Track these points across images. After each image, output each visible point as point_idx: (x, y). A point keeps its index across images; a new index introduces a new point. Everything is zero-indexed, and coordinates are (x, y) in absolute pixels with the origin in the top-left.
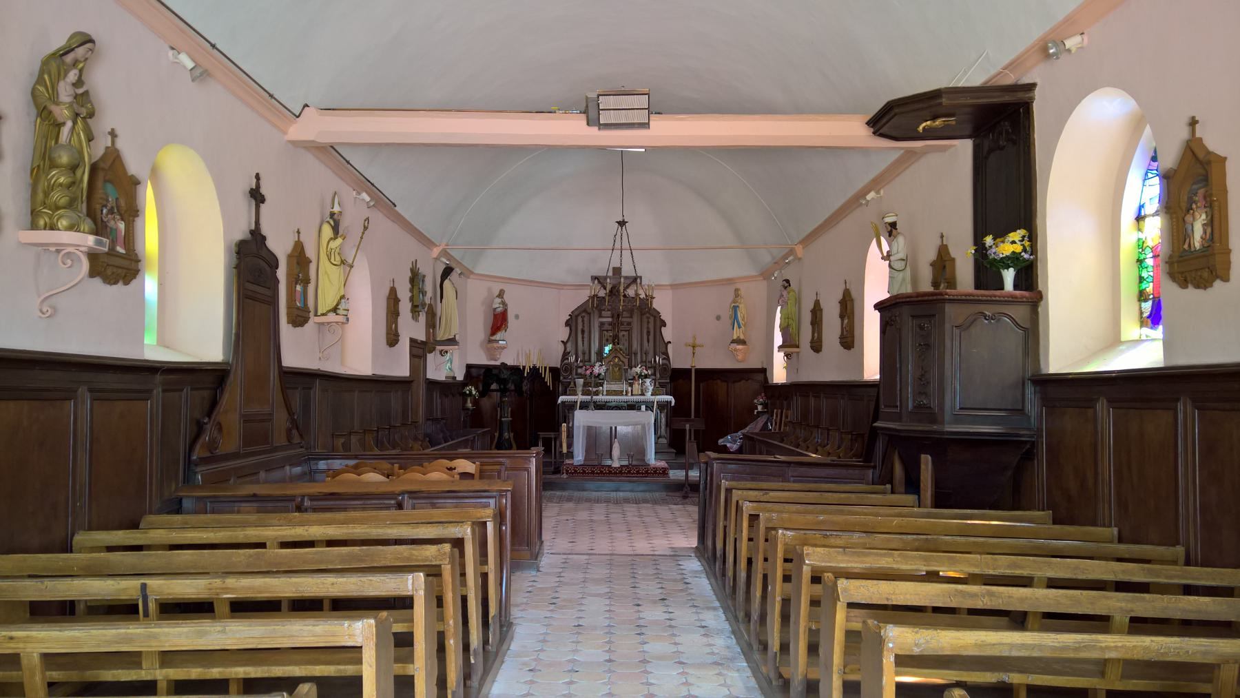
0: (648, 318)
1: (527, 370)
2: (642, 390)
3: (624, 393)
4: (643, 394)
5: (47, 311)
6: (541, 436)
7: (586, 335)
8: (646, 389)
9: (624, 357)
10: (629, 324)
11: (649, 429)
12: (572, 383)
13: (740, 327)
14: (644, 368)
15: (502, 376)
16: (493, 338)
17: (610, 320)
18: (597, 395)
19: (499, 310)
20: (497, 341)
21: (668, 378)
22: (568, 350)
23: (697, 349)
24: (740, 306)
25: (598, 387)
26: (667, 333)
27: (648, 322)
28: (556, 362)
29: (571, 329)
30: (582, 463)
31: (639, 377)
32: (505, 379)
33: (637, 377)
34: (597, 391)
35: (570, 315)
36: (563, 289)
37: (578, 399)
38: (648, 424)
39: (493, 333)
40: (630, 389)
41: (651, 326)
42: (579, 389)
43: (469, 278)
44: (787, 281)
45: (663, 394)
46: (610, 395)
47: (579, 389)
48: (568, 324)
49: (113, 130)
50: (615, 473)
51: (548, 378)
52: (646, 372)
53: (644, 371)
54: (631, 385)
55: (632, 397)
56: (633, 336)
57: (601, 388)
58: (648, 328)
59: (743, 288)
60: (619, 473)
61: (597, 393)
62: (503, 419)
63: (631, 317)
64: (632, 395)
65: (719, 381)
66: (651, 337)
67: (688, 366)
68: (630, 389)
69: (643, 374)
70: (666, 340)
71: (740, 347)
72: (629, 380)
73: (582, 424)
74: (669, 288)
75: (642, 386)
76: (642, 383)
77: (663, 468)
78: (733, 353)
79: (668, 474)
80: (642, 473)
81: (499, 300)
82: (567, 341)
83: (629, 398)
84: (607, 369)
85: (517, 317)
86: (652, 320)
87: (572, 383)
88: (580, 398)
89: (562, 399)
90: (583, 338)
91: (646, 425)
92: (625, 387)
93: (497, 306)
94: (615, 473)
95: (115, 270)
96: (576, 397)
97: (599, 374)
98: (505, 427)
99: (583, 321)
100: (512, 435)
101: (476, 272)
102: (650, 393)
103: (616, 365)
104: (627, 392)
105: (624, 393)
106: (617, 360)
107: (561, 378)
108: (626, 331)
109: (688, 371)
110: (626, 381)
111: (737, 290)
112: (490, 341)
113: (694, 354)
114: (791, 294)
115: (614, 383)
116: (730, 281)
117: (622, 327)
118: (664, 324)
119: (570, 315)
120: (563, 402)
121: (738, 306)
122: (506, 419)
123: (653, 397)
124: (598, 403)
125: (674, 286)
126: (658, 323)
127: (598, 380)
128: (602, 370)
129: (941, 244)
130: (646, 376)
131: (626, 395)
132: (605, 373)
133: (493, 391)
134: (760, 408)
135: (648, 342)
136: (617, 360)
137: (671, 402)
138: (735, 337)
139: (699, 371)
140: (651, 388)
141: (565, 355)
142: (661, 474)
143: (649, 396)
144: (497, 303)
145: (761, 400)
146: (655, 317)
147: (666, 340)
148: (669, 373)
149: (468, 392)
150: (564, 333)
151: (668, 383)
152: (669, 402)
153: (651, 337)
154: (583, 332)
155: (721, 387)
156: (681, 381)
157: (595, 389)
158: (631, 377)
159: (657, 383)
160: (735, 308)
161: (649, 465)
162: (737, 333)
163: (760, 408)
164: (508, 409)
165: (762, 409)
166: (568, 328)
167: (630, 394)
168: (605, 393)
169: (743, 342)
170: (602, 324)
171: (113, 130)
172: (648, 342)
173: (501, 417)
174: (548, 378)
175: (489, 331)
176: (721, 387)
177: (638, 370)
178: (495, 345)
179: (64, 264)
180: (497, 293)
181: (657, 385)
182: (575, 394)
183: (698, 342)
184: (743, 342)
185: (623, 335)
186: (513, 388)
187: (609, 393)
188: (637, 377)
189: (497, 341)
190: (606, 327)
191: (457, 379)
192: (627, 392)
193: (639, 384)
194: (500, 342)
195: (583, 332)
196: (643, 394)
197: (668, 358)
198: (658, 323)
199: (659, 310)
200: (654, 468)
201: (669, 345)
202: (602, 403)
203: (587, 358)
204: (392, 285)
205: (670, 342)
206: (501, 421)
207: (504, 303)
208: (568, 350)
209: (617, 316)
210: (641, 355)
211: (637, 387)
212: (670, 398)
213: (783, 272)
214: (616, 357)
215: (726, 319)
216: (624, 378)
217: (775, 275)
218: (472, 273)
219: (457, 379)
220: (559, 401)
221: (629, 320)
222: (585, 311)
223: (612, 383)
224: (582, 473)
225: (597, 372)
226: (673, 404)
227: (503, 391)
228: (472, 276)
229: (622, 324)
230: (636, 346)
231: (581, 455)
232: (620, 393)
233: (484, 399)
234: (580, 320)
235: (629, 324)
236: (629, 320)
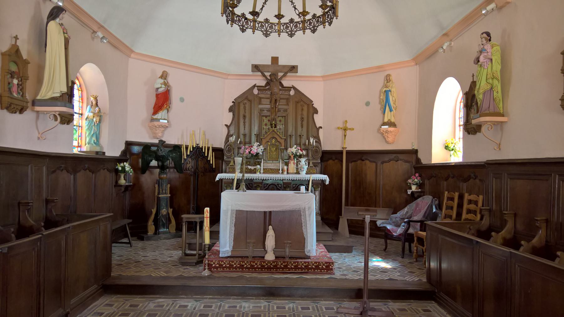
0: (302, 106)
1: (190, 148)
2: (297, 169)
3: (281, 172)
4: (298, 173)
5: (44, 137)
6: (184, 220)
7: (247, 120)
8: (302, 168)
9: (281, 138)
10: (286, 110)
11: (310, 215)
12: (232, 162)
13: (391, 110)
14: (299, 148)
15: (160, 153)
16: (155, 117)
17: (269, 106)
18: (255, 173)
19: (161, 90)
20: (158, 120)
21: (319, 159)
22: (231, 133)
23: (348, 132)
24: (392, 90)
25: (256, 165)
26: (319, 120)
27: (302, 110)
28: (220, 144)
29: (234, 115)
30: (229, 254)
31: (294, 157)
32: (163, 157)
33: (292, 157)
34: (255, 169)
35: (233, 102)
36: (227, 79)
37: (235, 177)
38: (309, 208)
39: (155, 112)
40: (285, 168)
41: (305, 113)
42: (238, 167)
43: (130, 57)
44: (488, 34)
45: (317, 173)
46: (267, 173)
47: (238, 167)
48: (231, 109)
49: (17, 36)
50: (269, 268)
51: (211, 157)
52: (301, 153)
53: (300, 151)
54: (287, 164)
55: (288, 176)
56: (289, 121)
57: (259, 166)
58: (302, 114)
59: (394, 75)
60: (273, 268)
61: (254, 172)
62: (160, 196)
63: (288, 104)
64: (288, 173)
65: (367, 162)
66: (305, 123)
67: (338, 148)
68: (285, 168)
69: (298, 154)
70: (318, 126)
71: (392, 129)
72: (285, 160)
73: (230, 207)
74: (321, 79)
75: (297, 166)
76: (297, 162)
77: (326, 263)
78: (383, 135)
79: (332, 269)
80: (302, 268)
81: (162, 81)
82: (230, 125)
83: (285, 176)
84: (265, 149)
85: (182, 100)
86: (305, 108)
87: (232, 162)
88: (237, 175)
89: (219, 176)
90: (244, 123)
91: (306, 210)
92: (281, 165)
93: (159, 86)
94: (269, 268)
95: (15, 106)
96: (233, 175)
97: (257, 154)
98: (163, 204)
99: (245, 108)
100: (170, 211)
101: (136, 51)
102: (305, 172)
103: (273, 145)
104: (283, 170)
105: (281, 172)
106: (274, 141)
107: (225, 158)
108: (282, 117)
109: (340, 153)
110: (283, 160)
111: (389, 75)
112: (153, 120)
113: (345, 136)
114: (495, 48)
115: (272, 162)
116: (380, 68)
117: (279, 114)
118: (316, 111)
119: (233, 102)
120: (221, 180)
121: (390, 91)
122: (163, 196)
123: (308, 176)
124: (255, 181)
125: (325, 78)
126: (311, 111)
127: (255, 159)
128: (260, 150)
129: (472, 81)
130: (300, 156)
131: (282, 173)
132: (263, 152)
133: (154, 167)
134: (414, 188)
135: (302, 127)
136: (274, 141)
137: (325, 180)
138: (386, 120)
139: (349, 153)
140: (306, 167)
141: (229, 136)
142: (324, 269)
143: (303, 175)
144: (159, 83)
145: (416, 180)
146: (308, 105)
147: (318, 126)
148: (320, 155)
149: (120, 168)
150: (228, 118)
151: (318, 163)
152: (323, 181)
153: (305, 123)
154: (244, 117)
155: (369, 167)
156: (331, 162)
157: (252, 168)
158: (286, 158)
159: (311, 163)
160: (387, 93)
161: (309, 257)
162: (388, 116)
163: (414, 188)
164: (166, 186)
165: (416, 189)
166: (231, 114)
167: (286, 173)
168: (262, 171)
169: (391, 124)
170: (262, 110)
171: (17, 36)
172: (302, 127)
173: (159, 194)
174: (211, 157)
175: (152, 111)
176: (369, 167)
177: (293, 150)
178: (156, 123)
179: (50, 118)
180: (160, 74)
181: (311, 165)
182: (234, 172)
183: (349, 126)
184: (391, 124)
185: (280, 121)
186: (172, 165)
187: (266, 171)
188: (292, 157)
189: (158, 120)
190: (266, 113)
191: (106, 154)
192: (283, 170)
193: (294, 163)
194: (161, 121)
195: (244, 117)
196: (298, 173)
197: (318, 141)
198: (311, 111)
199: (312, 100)
200: (316, 263)
201: (320, 130)
202: (258, 181)
203: (247, 140)
204: (14, 43)
205: (321, 127)
206: (159, 199)
207: (166, 84)
208: (231, 133)
209: (274, 109)
210: (296, 138)
211: (292, 166)
212: (325, 177)
213: (453, 43)
214: (273, 138)
215: (376, 106)
216: (280, 157)
217: (444, 47)
218: (132, 51)
219: (106, 154)
220: (217, 179)
221: (285, 107)
222: (247, 98)
223: (269, 162)
224: (229, 268)
225: (256, 151)
226: (327, 183)
227: (163, 168)
228: (132, 55)
229: (279, 111)
230: (291, 130)
231: (228, 245)
232: (276, 171)
233: (144, 175)
234: (242, 107)
235: (286, 110)
236: (285, 107)
